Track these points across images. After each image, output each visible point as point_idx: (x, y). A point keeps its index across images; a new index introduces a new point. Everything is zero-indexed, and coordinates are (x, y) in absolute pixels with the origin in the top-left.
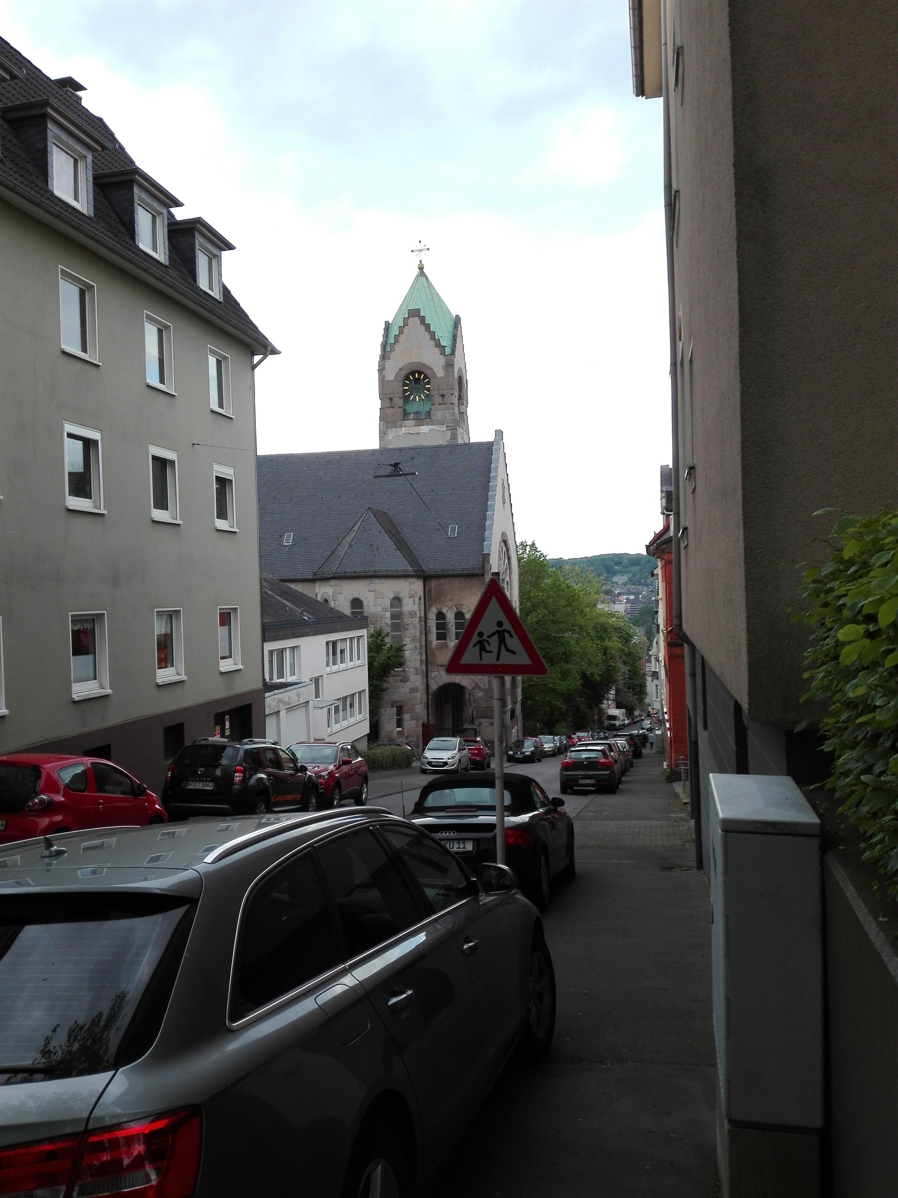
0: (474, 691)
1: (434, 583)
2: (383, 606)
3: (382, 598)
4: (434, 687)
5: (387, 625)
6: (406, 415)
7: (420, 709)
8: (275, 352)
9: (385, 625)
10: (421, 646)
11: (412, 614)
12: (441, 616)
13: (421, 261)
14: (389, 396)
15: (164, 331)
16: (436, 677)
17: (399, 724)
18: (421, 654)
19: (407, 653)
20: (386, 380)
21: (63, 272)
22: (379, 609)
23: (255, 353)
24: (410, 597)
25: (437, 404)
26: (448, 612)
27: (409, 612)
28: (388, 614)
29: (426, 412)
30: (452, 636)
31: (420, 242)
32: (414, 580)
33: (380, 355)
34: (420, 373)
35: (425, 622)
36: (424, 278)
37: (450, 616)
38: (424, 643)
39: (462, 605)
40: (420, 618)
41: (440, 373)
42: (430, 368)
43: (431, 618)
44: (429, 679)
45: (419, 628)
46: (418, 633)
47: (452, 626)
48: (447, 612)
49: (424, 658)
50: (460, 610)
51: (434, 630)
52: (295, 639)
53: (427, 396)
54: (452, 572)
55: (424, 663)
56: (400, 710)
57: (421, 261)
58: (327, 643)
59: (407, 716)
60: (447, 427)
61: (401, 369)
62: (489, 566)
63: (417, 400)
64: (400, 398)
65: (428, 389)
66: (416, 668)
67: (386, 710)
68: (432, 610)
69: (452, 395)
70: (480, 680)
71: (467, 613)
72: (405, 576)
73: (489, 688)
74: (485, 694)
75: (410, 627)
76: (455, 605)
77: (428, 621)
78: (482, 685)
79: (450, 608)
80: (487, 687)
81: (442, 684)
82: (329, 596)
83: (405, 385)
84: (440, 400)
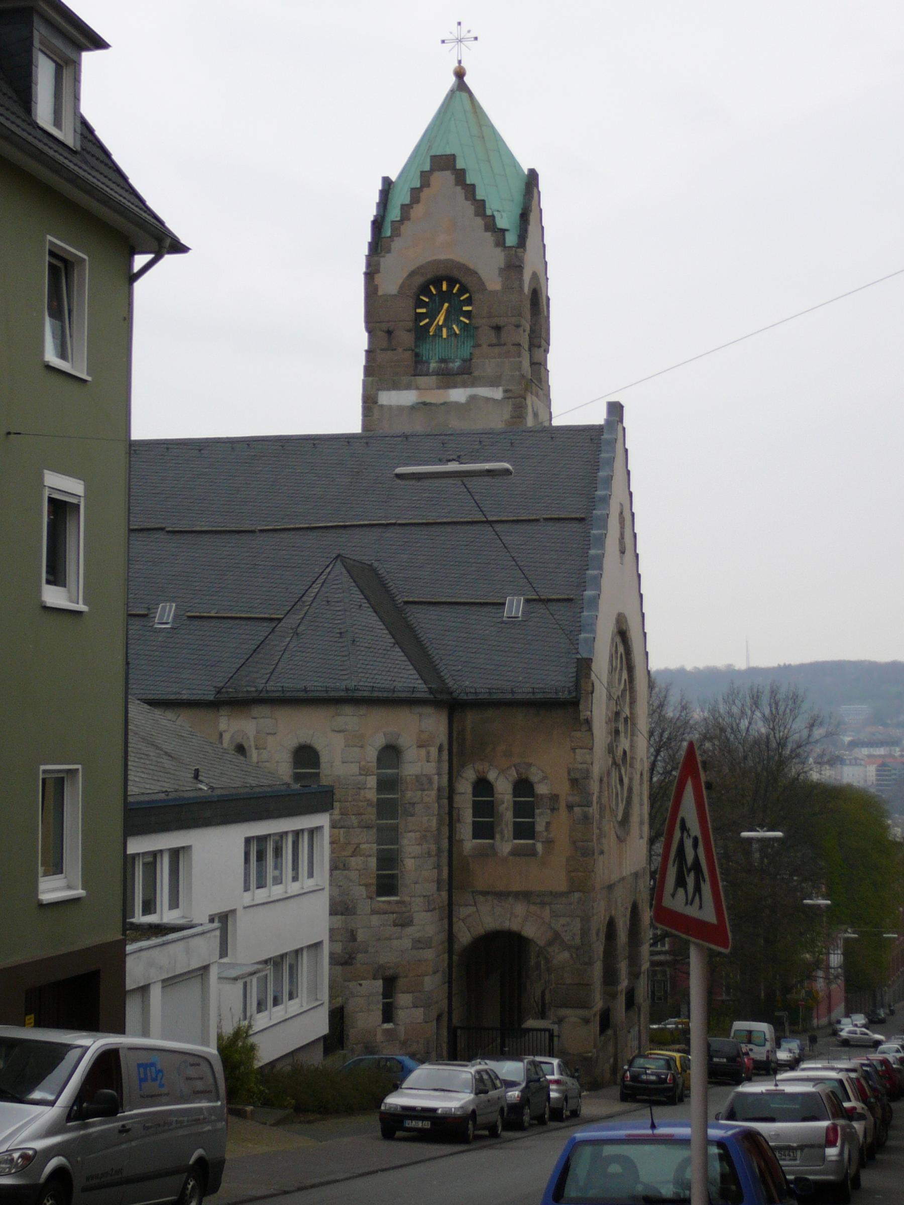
0: (550, 950)
1: (471, 718)
2: (363, 763)
3: (362, 747)
4: (464, 937)
7: (432, 983)
8: (178, 248)
9: (366, 803)
10: (439, 850)
11: (422, 782)
12: (483, 786)
13: (460, 62)
14: (385, 326)
16: (469, 916)
17: (388, 1014)
18: (438, 867)
19: (409, 864)
20: (380, 293)
22: (354, 769)
25: (485, 346)
27: (417, 776)
28: (372, 781)
29: (464, 361)
31: (459, 24)
32: (429, 710)
34: (452, 282)
35: (451, 799)
37: (503, 788)
38: (445, 844)
39: (530, 765)
40: (439, 790)
41: (493, 281)
42: (474, 273)
43: (463, 791)
44: (455, 920)
47: (507, 809)
48: (497, 779)
50: (524, 777)
51: (468, 816)
53: (465, 328)
54: (509, 696)
56: (390, 984)
57: (460, 62)
58: (248, 841)
59: (403, 999)
60: (505, 391)
61: (412, 274)
63: (445, 336)
64: (409, 331)
65: (468, 314)
66: (428, 896)
67: (361, 985)
68: (464, 775)
69: (518, 326)
70: (563, 926)
71: (539, 782)
72: (409, 702)
73: (582, 944)
74: (574, 956)
75: (419, 809)
77: (457, 798)
78: (567, 937)
79: (502, 771)
80: (578, 941)
81: (480, 931)
83: (420, 304)
84: (491, 336)
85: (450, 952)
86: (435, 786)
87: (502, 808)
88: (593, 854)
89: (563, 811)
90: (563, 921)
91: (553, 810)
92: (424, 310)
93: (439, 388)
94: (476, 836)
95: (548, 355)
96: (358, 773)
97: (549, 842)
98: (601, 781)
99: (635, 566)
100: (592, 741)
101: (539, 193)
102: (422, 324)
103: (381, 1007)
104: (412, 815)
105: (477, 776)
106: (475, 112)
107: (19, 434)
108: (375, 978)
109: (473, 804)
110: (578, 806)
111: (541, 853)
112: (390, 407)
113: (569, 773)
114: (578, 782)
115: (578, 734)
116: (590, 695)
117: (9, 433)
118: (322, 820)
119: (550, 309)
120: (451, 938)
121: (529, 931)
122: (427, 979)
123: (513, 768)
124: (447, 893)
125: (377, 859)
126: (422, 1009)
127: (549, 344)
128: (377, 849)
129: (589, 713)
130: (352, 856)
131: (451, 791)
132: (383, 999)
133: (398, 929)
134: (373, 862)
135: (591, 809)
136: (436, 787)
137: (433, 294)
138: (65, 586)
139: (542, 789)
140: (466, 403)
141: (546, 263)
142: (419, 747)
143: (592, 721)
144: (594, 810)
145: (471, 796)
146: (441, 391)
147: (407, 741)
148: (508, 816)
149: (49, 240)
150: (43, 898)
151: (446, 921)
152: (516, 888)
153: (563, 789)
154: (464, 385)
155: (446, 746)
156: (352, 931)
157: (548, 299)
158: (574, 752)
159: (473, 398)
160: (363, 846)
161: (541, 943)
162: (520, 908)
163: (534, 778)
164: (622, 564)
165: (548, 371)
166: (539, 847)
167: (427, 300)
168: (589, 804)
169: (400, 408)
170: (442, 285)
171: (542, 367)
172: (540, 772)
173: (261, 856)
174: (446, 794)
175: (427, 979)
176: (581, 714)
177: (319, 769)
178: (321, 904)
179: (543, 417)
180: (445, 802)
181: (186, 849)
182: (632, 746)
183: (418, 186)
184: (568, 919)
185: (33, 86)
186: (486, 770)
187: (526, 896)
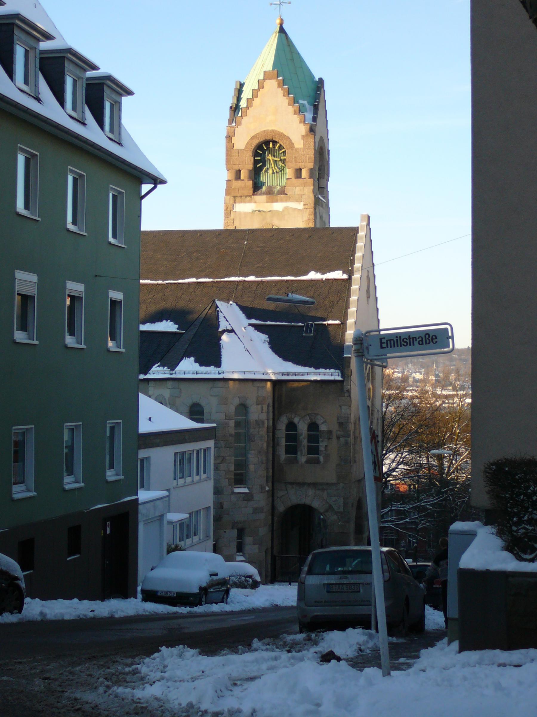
4: (281, 508)
5: (231, 435)
6: (257, 187)
7: (263, 531)
8: (163, 182)
10: (267, 460)
11: (259, 423)
12: (291, 426)
15: (79, 179)
18: (267, 469)
19: (252, 467)
21: (20, 148)
23: (143, 183)
24: (257, 404)
26: (300, 422)
27: (256, 421)
28: (232, 423)
30: (303, 451)
33: (229, 120)
34: (275, 142)
35: (274, 433)
36: (283, 35)
37: (303, 427)
38: (271, 457)
39: (317, 414)
40: (268, 427)
43: (280, 429)
45: (266, 440)
46: (265, 445)
48: (299, 422)
49: (270, 474)
50: (313, 421)
51: (283, 442)
52: (146, 450)
55: (270, 480)
56: (241, 533)
58: (176, 454)
59: (248, 539)
60: (305, 205)
61: (253, 138)
62: (350, 371)
67: (225, 532)
71: (322, 423)
76: (308, 415)
77: (277, 432)
80: (342, 510)
81: (290, 504)
82: (165, 399)
85: (273, 515)
86: (266, 426)
87: (301, 438)
88: (350, 462)
89: (334, 439)
90: (334, 499)
91: (329, 439)
92: (259, 158)
93: (267, 202)
94: (287, 453)
95: (328, 182)
96: (225, 419)
97: (327, 457)
98: (355, 423)
99: (376, 304)
100: (350, 402)
101: (324, 91)
102: (258, 166)
103: (236, 543)
104: (253, 441)
105: (288, 421)
106: (289, 45)
107: (101, 276)
108: (233, 528)
109: (286, 436)
110: (343, 437)
111: (322, 462)
112: (240, 213)
113: (338, 419)
114: (343, 424)
115: (343, 398)
116: (350, 377)
117: (96, 276)
118: (210, 444)
119: (330, 156)
120: (273, 507)
121: (316, 504)
122: (260, 529)
123: (308, 416)
124: (271, 483)
125: (234, 465)
126: (258, 545)
127: (329, 177)
128: (235, 460)
129: (349, 387)
130: (221, 463)
131: (274, 429)
132: (237, 540)
133: (246, 502)
134: (232, 468)
135: (349, 439)
136: (266, 426)
137: (264, 149)
138: (115, 341)
139: (323, 428)
140: (282, 211)
141: (328, 130)
142: (257, 404)
143: (351, 391)
144: (351, 439)
145: (285, 431)
146: (269, 204)
147: (251, 402)
148: (305, 442)
149: (111, 187)
150: (109, 479)
151: (271, 498)
152: (308, 480)
153: (335, 427)
154: (282, 201)
155: (271, 405)
156: (221, 503)
157: (329, 151)
158: (341, 408)
159: (286, 208)
160: (227, 458)
161: (322, 511)
162: (311, 492)
163: (319, 422)
164: (368, 304)
165: (328, 192)
166: (321, 459)
167: (261, 153)
168: (348, 436)
169: (246, 214)
170: (269, 144)
171: (325, 189)
172: (322, 418)
173: (182, 462)
174: (271, 430)
175: (260, 529)
176: (345, 387)
177: (204, 416)
178: (208, 487)
179: (324, 223)
180: (271, 434)
181: (148, 458)
182: (373, 404)
183: (257, 88)
184: (337, 498)
185: (104, 118)
186: (293, 417)
187: (314, 485)
